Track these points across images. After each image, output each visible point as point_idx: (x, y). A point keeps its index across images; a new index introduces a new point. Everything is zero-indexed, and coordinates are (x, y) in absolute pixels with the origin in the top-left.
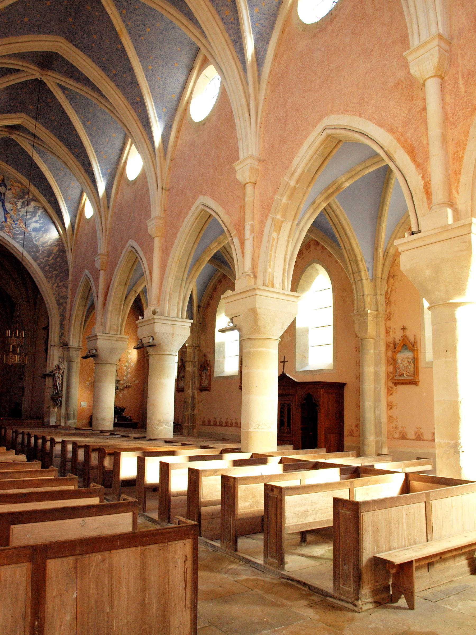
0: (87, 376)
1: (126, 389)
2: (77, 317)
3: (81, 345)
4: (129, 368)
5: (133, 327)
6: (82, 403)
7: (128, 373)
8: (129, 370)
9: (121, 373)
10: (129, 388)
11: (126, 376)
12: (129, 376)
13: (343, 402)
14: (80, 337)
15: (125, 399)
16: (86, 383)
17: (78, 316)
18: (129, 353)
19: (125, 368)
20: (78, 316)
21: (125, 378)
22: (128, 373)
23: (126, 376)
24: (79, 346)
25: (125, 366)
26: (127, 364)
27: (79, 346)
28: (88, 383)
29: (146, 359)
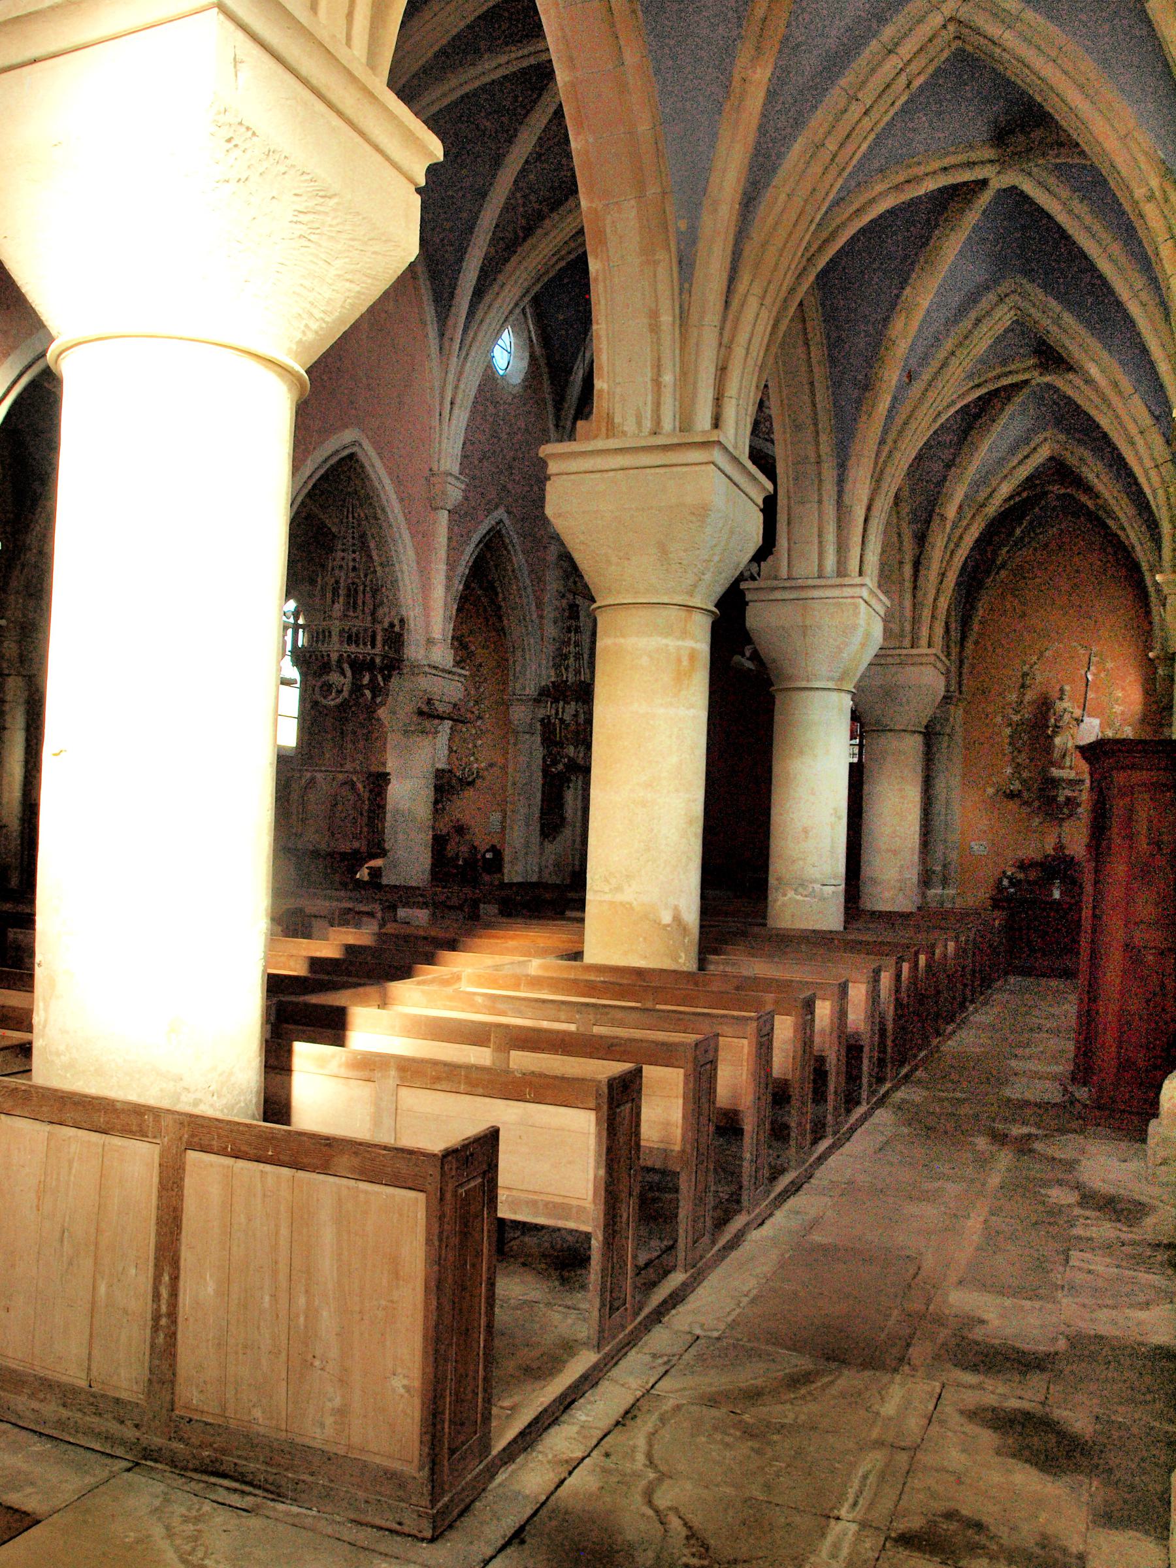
28: (990, 791)
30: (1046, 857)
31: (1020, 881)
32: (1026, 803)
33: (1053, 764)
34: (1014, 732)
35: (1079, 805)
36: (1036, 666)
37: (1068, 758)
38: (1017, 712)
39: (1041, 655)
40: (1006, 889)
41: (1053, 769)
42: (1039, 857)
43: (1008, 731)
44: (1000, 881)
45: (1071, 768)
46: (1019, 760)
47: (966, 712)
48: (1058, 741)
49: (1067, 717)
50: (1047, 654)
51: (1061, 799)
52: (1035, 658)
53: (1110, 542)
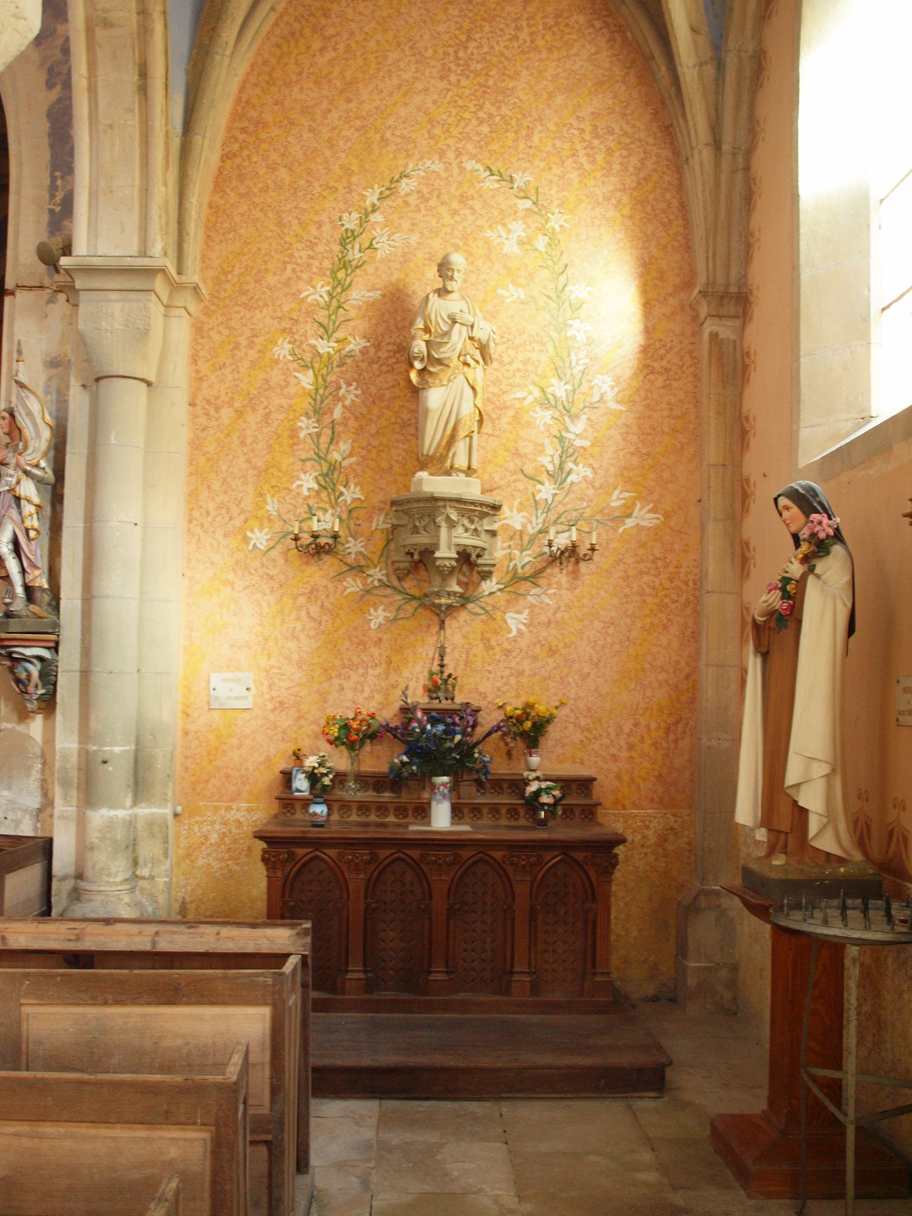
0: (251, 489)
1: (559, 576)
2: (100, 33)
3: (157, 249)
4: (574, 418)
5: (595, 115)
6: (216, 680)
7: (567, 452)
8: (579, 427)
9: (517, 454)
10: (583, 566)
11: (559, 475)
12: (579, 473)
13: (190, 953)
14: (146, 192)
15: (552, 652)
16: (246, 540)
17: (107, 24)
18: (576, 308)
19: (544, 417)
20: (107, 24)
21: (546, 491)
22: (567, 452)
23: (559, 475)
24: (144, 254)
25: (546, 402)
26: (559, 390)
27: (144, 254)
28: (260, 538)
29: (706, 336)
30: (406, 710)
31: (340, 778)
32: (357, 569)
33: (424, 463)
34: (322, 382)
35: (486, 575)
36: (377, 217)
37: (461, 447)
38: (327, 332)
39: (390, 192)
40: (306, 803)
41: (423, 475)
42: (389, 715)
43: (307, 380)
44: (287, 777)
45: (469, 471)
46: (336, 456)
47: (198, 330)
48: (435, 398)
49: (458, 336)
50: (406, 186)
51: (445, 553)
52: (372, 197)
53: (487, 144)
